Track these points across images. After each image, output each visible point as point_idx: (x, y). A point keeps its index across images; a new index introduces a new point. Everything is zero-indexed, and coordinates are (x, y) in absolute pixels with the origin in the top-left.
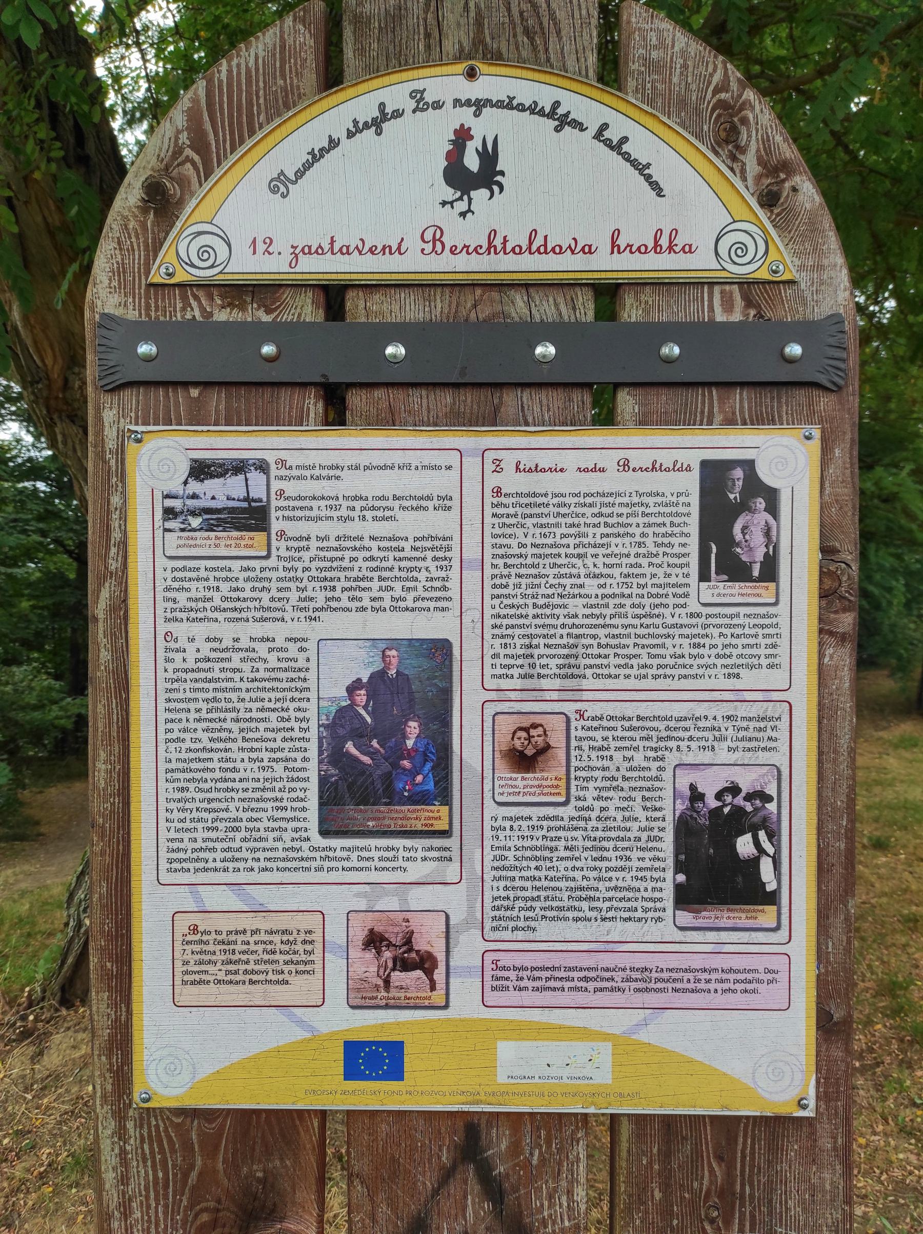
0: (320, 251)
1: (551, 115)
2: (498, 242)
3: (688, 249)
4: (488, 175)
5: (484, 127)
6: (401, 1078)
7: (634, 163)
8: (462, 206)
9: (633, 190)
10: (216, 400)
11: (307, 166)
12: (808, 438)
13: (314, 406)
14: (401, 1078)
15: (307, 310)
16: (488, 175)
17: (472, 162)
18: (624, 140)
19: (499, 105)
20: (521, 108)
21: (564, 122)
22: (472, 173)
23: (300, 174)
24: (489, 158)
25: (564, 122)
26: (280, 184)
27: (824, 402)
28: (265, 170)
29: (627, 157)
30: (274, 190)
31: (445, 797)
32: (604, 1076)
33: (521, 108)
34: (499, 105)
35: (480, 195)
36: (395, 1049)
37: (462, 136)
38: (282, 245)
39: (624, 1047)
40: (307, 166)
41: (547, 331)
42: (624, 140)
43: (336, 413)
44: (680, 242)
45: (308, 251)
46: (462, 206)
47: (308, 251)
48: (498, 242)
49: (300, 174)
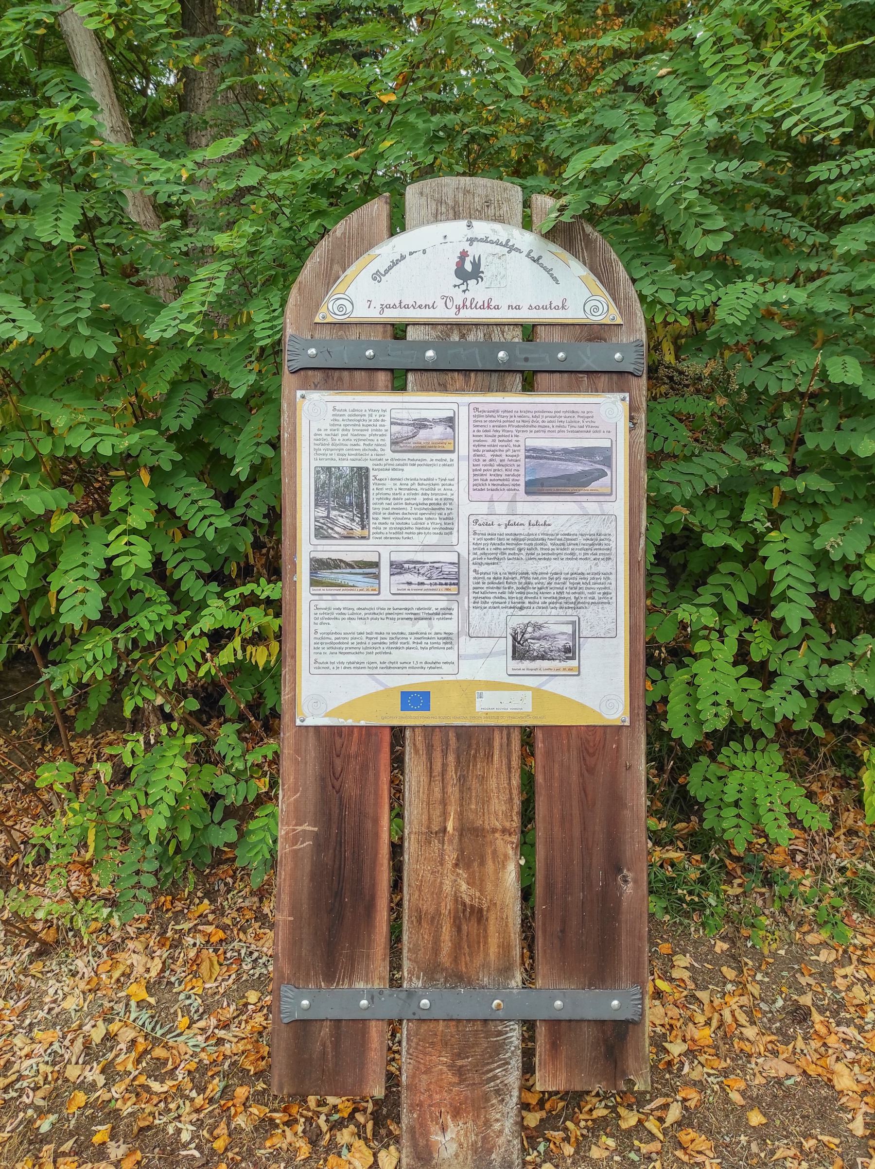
0: (394, 307)
1: (506, 245)
2: (468, 304)
3: (497, 308)
4: (476, 274)
5: (475, 251)
6: (428, 708)
7: (545, 268)
8: (464, 287)
9: (532, 280)
10: (459, 378)
11: (390, 268)
12: (303, 397)
13: (382, 378)
14: (428, 708)
15: (515, 336)
16: (476, 274)
17: (468, 267)
18: (540, 258)
19: (481, 240)
20: (492, 242)
21: (512, 249)
22: (468, 272)
23: (386, 272)
24: (476, 265)
25: (512, 249)
26: (377, 276)
27: (634, 381)
28: (372, 268)
29: (542, 266)
30: (374, 279)
31: (275, 572)
32: (529, 708)
33: (492, 242)
34: (481, 240)
35: (472, 282)
36: (426, 695)
37: (464, 255)
38: (376, 304)
39: (538, 693)
40: (390, 268)
41: (370, 345)
42: (540, 258)
43: (529, 384)
44: (493, 304)
45: (388, 307)
46: (464, 287)
47: (388, 307)
48: (468, 304)
49: (386, 272)
